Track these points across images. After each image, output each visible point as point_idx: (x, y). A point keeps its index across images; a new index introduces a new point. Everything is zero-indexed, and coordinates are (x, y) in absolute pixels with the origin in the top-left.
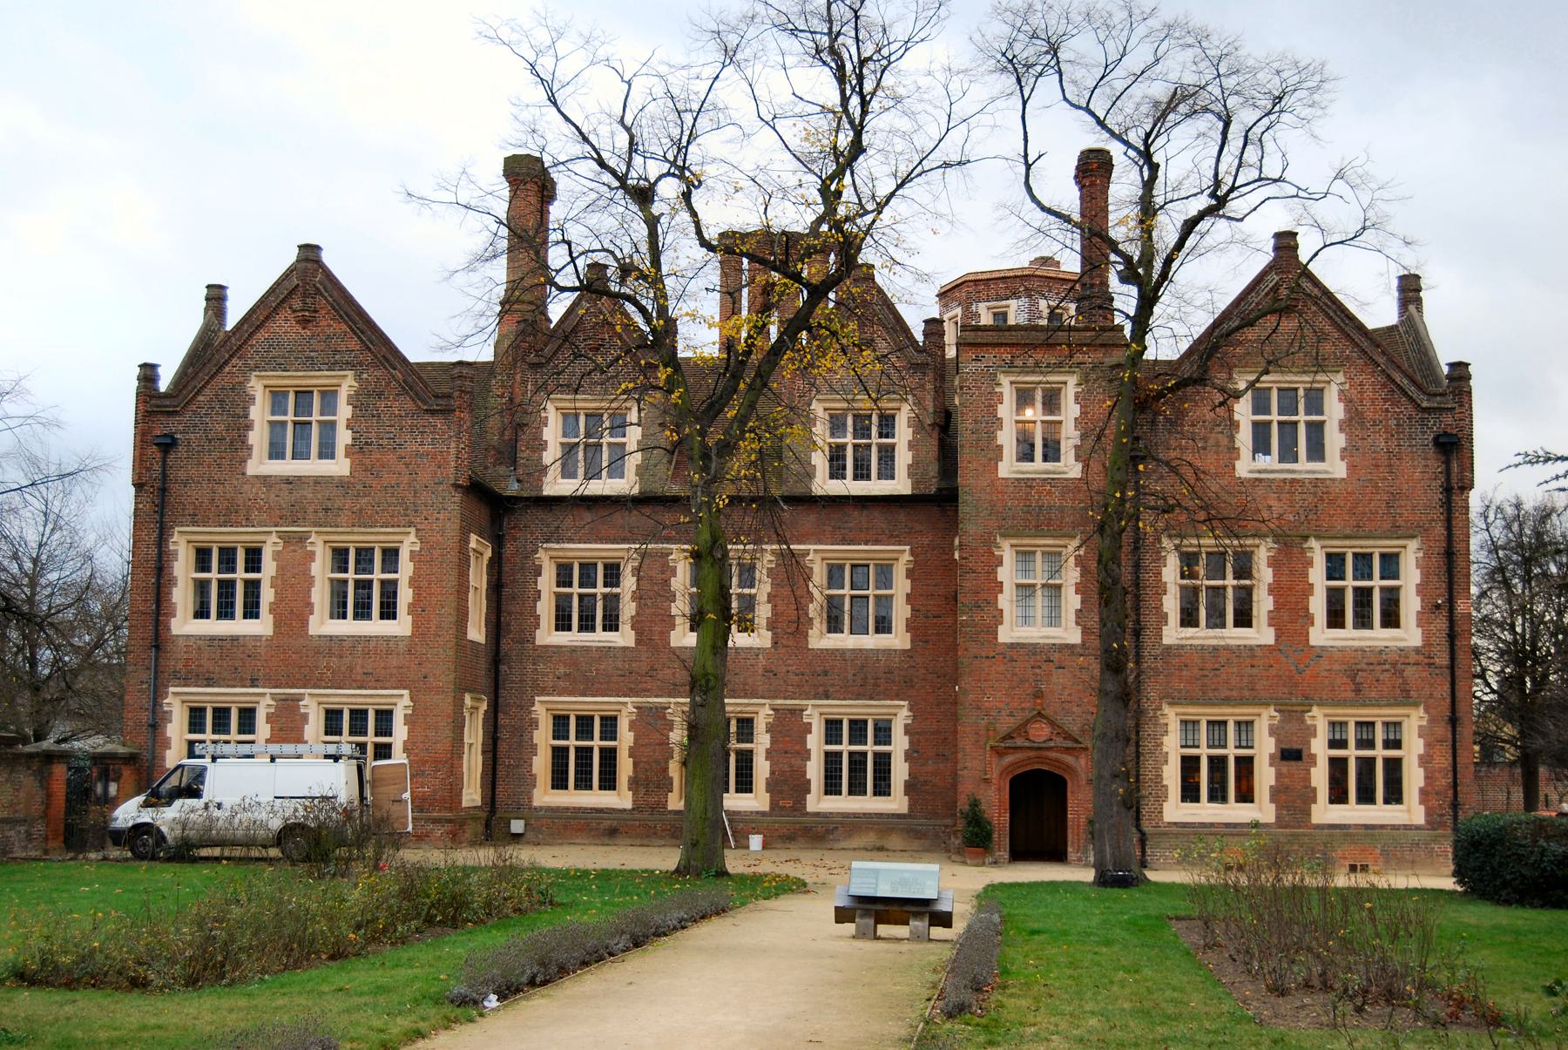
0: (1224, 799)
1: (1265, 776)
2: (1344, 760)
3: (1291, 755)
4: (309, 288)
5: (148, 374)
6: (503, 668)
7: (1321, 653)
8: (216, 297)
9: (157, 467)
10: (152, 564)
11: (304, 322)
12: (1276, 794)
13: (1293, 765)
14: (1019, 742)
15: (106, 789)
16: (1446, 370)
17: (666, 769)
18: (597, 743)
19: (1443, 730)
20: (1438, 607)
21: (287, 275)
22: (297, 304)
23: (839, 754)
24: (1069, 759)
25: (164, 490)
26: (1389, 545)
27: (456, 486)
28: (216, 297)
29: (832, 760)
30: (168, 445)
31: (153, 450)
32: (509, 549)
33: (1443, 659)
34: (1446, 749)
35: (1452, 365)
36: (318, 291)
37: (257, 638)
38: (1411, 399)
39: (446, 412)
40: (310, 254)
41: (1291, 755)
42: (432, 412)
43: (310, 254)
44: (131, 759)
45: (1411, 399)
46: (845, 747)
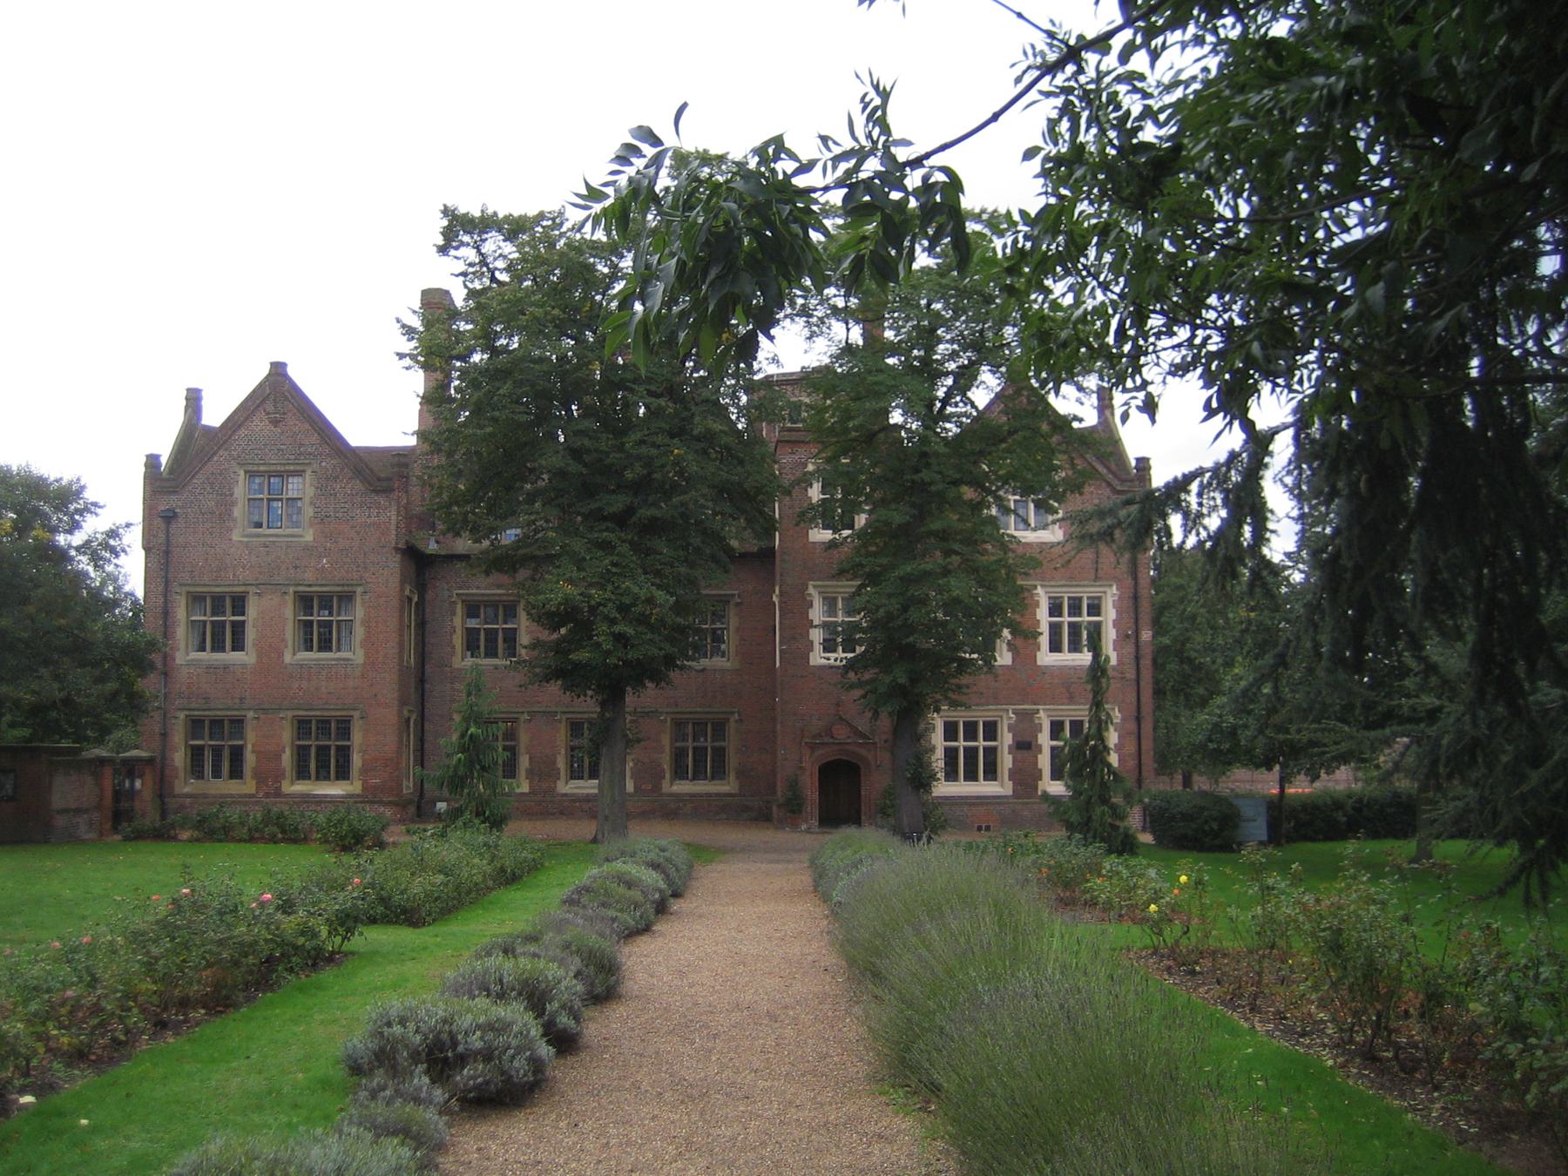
0: (956, 779)
1: (1006, 761)
2: (956, 750)
3: (1025, 746)
4: (278, 396)
5: (152, 462)
6: (427, 686)
7: (1045, 670)
8: (194, 400)
9: (162, 536)
10: (159, 610)
11: (275, 423)
12: (1013, 774)
13: (1025, 754)
14: (826, 740)
15: (132, 784)
16: (1133, 463)
17: (554, 763)
18: (981, 743)
19: (1133, 726)
20: (1128, 636)
21: (261, 385)
22: (270, 408)
23: (956, 750)
24: (863, 752)
25: (167, 553)
26: (1094, 591)
27: (397, 549)
28: (194, 400)
29: (951, 754)
30: (170, 517)
31: (158, 522)
32: (429, 595)
33: (1131, 675)
34: (1133, 739)
35: (1138, 460)
36: (286, 399)
37: (244, 666)
38: (1109, 484)
39: (387, 491)
40: (278, 369)
41: (1025, 746)
42: (376, 492)
43: (278, 369)
44: (150, 761)
45: (1109, 484)
46: (962, 743)
